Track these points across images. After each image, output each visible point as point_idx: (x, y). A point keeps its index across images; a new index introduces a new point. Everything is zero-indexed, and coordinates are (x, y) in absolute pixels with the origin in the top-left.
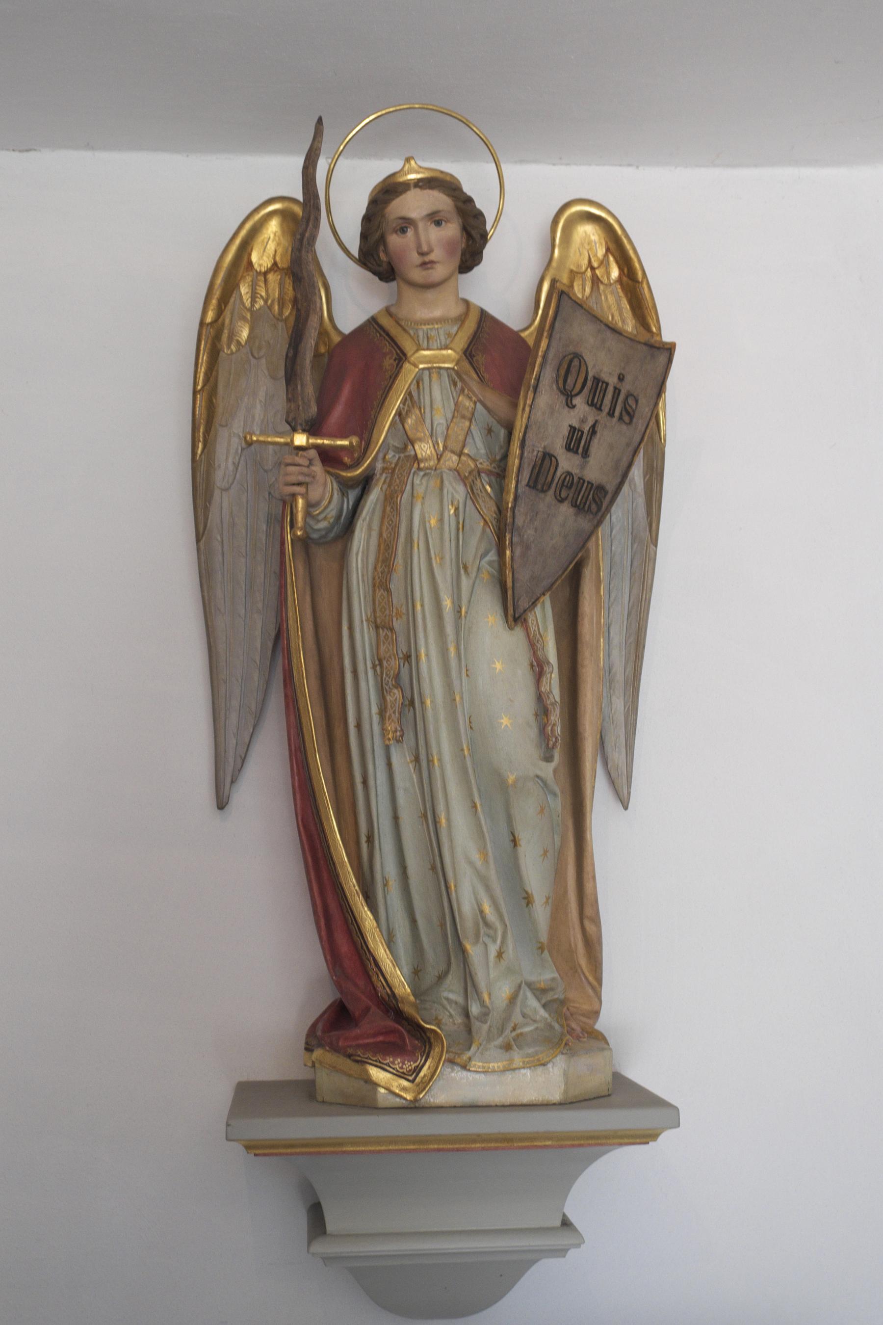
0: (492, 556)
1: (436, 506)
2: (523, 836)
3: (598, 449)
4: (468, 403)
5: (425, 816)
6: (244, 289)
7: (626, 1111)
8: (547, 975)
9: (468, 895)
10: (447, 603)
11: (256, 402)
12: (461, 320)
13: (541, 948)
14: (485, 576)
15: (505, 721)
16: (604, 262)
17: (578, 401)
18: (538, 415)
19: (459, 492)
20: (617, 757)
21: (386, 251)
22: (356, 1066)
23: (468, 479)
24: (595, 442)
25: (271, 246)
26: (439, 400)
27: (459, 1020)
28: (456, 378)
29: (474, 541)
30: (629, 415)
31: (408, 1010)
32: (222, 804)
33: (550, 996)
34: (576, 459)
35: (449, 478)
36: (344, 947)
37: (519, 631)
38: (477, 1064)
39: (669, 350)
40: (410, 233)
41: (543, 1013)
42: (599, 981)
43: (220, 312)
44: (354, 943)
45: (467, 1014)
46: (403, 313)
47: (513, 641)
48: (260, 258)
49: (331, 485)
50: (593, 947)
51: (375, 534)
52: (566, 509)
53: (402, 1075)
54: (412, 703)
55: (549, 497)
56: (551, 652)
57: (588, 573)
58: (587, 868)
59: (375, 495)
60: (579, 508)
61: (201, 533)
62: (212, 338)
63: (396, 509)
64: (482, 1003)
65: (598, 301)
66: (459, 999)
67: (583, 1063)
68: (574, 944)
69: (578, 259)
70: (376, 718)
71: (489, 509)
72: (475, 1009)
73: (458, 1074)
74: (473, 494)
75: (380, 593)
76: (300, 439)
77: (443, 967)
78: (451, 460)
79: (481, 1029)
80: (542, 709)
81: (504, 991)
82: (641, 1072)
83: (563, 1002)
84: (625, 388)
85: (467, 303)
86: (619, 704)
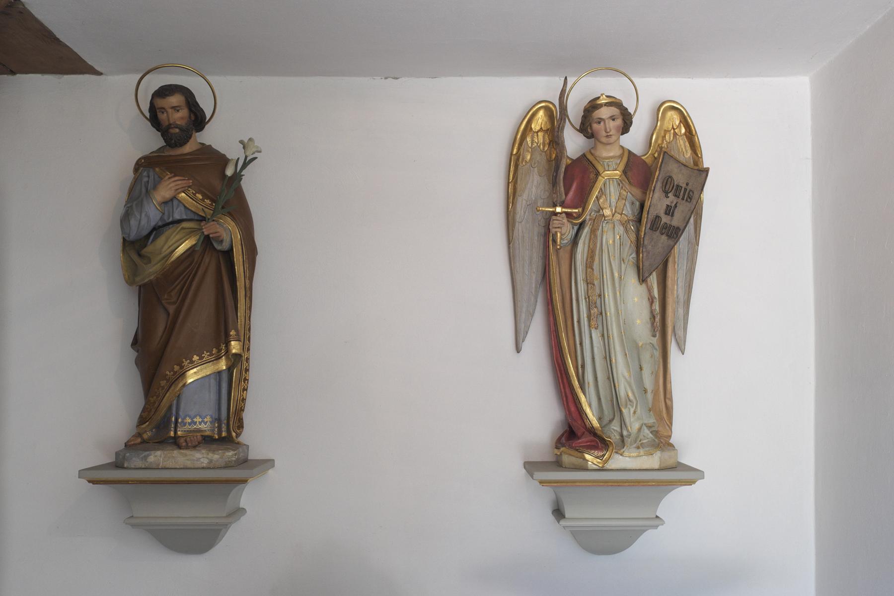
0: (634, 255)
1: (612, 236)
2: (645, 366)
3: (678, 214)
4: (625, 193)
5: (606, 358)
6: (529, 139)
7: (681, 475)
8: (652, 421)
9: (624, 389)
10: (616, 275)
11: (534, 186)
12: (621, 156)
13: (650, 410)
14: (631, 263)
15: (638, 321)
16: (679, 126)
17: (670, 195)
18: (654, 201)
19: (620, 229)
20: (680, 333)
21: (591, 129)
22: (579, 454)
23: (624, 224)
24: (676, 210)
25: (540, 121)
26: (613, 192)
27: (618, 437)
28: (620, 183)
29: (627, 249)
30: (690, 198)
31: (599, 433)
32: (518, 350)
33: (653, 429)
34: (669, 217)
35: (617, 223)
36: (573, 409)
37: (644, 285)
38: (626, 454)
39: (706, 171)
40: (602, 123)
41: (651, 435)
42: (671, 424)
43: (519, 149)
44: (577, 407)
45: (622, 436)
46: (597, 153)
47: (643, 288)
48: (535, 126)
49: (569, 226)
50: (669, 410)
51: (586, 246)
52: (664, 237)
53: (597, 457)
54: (601, 313)
55: (658, 233)
56: (656, 293)
57: (671, 260)
58: (668, 379)
59: (586, 230)
60: (669, 236)
61: (510, 240)
62: (515, 162)
63: (596, 236)
64: (628, 431)
65: (676, 143)
66: (618, 429)
67: (666, 455)
68: (662, 408)
69: (668, 125)
70: (586, 319)
71: (633, 236)
72: (625, 433)
73: (617, 456)
74: (626, 230)
75: (589, 270)
76: (559, 209)
77: (611, 417)
78: (618, 217)
79: (628, 441)
80: (653, 317)
81: (636, 426)
82: (686, 459)
83: (657, 432)
84: (689, 188)
85: (622, 147)
86: (681, 311)
